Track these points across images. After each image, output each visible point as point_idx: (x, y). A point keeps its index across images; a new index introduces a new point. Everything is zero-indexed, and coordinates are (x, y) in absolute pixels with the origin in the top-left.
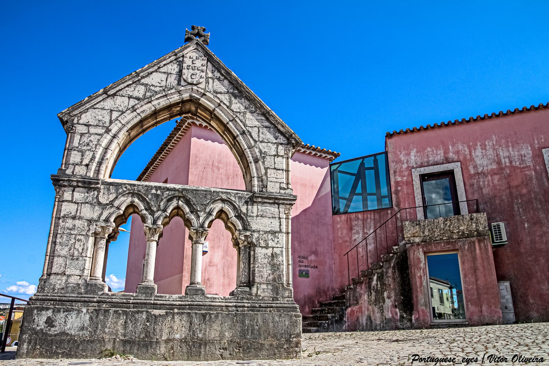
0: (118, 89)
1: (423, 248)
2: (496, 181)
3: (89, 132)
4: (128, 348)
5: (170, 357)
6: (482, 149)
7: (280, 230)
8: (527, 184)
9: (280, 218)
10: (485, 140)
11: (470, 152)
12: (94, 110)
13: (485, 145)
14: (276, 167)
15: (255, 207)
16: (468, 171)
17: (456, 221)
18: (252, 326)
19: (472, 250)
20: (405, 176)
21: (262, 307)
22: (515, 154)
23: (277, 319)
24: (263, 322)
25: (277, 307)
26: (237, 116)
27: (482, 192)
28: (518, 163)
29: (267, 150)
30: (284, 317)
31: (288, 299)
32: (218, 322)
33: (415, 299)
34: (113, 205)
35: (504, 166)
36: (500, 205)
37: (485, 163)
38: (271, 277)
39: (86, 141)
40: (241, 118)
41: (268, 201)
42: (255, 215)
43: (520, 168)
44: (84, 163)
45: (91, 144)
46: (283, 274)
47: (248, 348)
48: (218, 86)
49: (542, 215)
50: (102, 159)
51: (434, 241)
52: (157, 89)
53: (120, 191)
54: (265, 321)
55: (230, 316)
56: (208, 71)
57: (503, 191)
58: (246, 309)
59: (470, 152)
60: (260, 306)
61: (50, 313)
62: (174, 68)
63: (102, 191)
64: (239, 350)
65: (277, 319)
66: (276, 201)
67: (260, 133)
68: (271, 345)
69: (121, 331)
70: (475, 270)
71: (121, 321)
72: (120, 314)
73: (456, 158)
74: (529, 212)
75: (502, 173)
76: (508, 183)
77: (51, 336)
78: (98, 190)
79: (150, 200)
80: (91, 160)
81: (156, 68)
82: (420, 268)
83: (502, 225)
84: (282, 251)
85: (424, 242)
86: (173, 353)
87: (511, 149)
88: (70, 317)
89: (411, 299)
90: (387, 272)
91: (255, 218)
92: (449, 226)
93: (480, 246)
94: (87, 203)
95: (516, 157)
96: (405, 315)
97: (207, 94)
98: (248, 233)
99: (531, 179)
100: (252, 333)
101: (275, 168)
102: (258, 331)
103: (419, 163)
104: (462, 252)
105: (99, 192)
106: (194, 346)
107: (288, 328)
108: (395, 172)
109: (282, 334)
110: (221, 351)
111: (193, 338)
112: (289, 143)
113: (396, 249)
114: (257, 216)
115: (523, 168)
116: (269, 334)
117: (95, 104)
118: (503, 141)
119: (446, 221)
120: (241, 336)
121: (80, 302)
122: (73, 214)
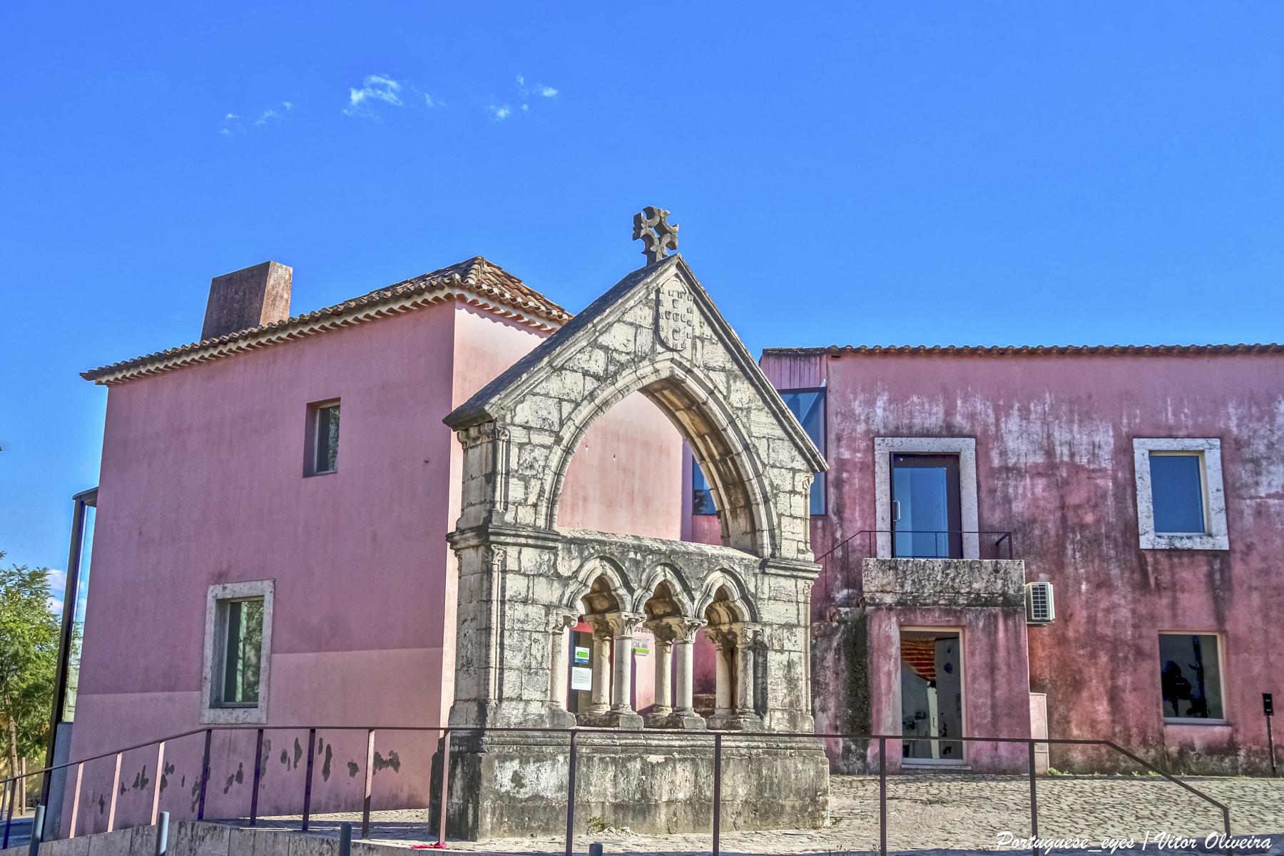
1: (898, 616)
2: (1039, 490)
3: (530, 443)
6: (1021, 417)
8: (1096, 506)
9: (798, 602)
10: (1030, 399)
11: (997, 420)
12: (534, 398)
13: (1028, 410)
16: (989, 460)
17: (967, 570)
19: (991, 632)
20: (859, 451)
22: (1082, 439)
23: (800, 766)
27: (1010, 508)
28: (1085, 460)
33: (874, 716)
35: (1058, 461)
36: (1041, 540)
37: (1023, 448)
38: (787, 700)
39: (529, 459)
40: (745, 420)
42: (766, 596)
43: (1088, 470)
44: (530, 502)
45: (536, 466)
49: (1115, 571)
50: (555, 495)
51: (922, 605)
52: (623, 358)
53: (586, 553)
54: (785, 767)
57: (1050, 511)
59: (997, 420)
61: (515, 765)
62: (644, 315)
63: (560, 553)
65: (800, 766)
68: (793, 807)
69: (611, 790)
70: (992, 669)
71: (610, 774)
72: (607, 763)
73: (967, 428)
74: (1092, 561)
75: (1054, 475)
76: (1062, 497)
77: (521, 801)
78: (553, 550)
80: (540, 496)
82: (890, 657)
83: (1050, 588)
85: (902, 604)
87: (1076, 427)
88: (543, 770)
89: (867, 716)
90: (823, 659)
92: (953, 580)
93: (1006, 625)
94: (541, 575)
95: (1084, 447)
96: (853, 747)
97: (695, 370)
98: (758, 628)
99: (1104, 496)
100: (771, 789)
101: (791, 516)
103: (891, 427)
104: (972, 631)
108: (839, 439)
113: (846, 613)
114: (769, 599)
115: (1094, 471)
118: (1064, 408)
119: (948, 568)
122: (524, 594)
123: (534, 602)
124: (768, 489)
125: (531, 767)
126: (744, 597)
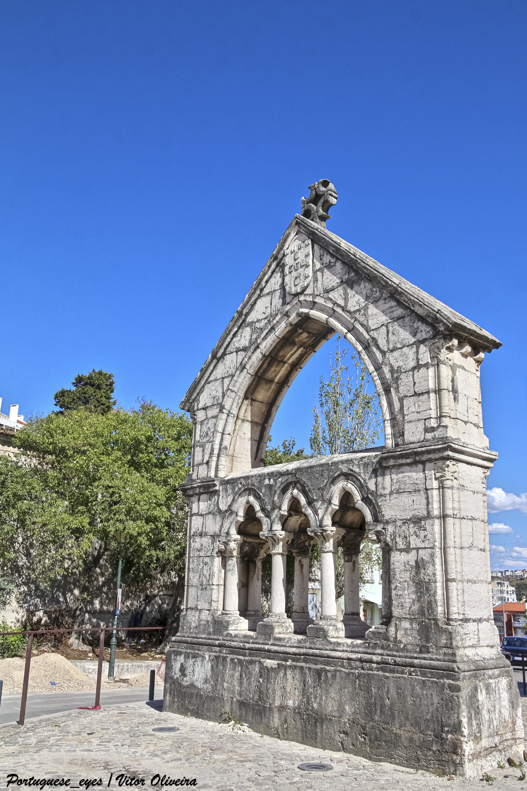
0: (225, 345)
4: (244, 713)
5: (284, 735)
7: (428, 513)
14: (417, 390)
15: (387, 478)
18: (382, 698)
21: (398, 665)
24: (398, 694)
25: (421, 667)
26: (356, 319)
29: (401, 363)
30: (429, 688)
31: (445, 650)
32: (336, 686)
34: (231, 510)
38: (416, 607)
41: (404, 461)
42: (387, 491)
46: (436, 601)
47: (377, 739)
48: (330, 279)
52: (262, 324)
53: (237, 489)
55: (351, 676)
56: (315, 261)
58: (374, 665)
60: (395, 661)
64: (365, 739)
66: (417, 458)
67: (390, 335)
68: (411, 740)
71: (237, 674)
79: (264, 495)
81: (258, 292)
84: (432, 555)
86: (287, 729)
91: (388, 497)
94: (210, 513)
97: (318, 300)
98: (379, 528)
100: (382, 711)
101: (416, 394)
102: (391, 709)
105: (219, 496)
106: (309, 722)
107: (437, 709)
109: (428, 721)
110: (341, 735)
111: (307, 709)
112: (436, 333)
114: (391, 493)
116: (407, 718)
117: (209, 377)
120: (367, 715)
121: (205, 645)
123: (206, 534)
124: (388, 376)
125: (191, 661)
126: (365, 500)
